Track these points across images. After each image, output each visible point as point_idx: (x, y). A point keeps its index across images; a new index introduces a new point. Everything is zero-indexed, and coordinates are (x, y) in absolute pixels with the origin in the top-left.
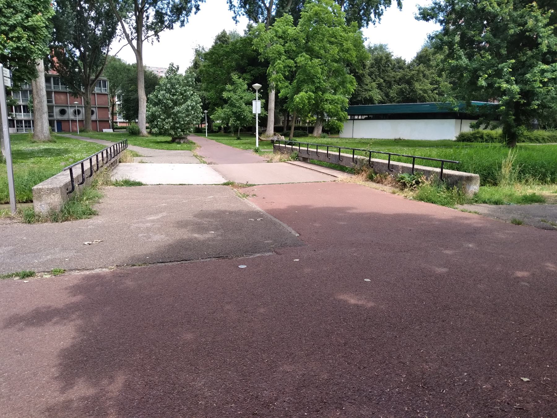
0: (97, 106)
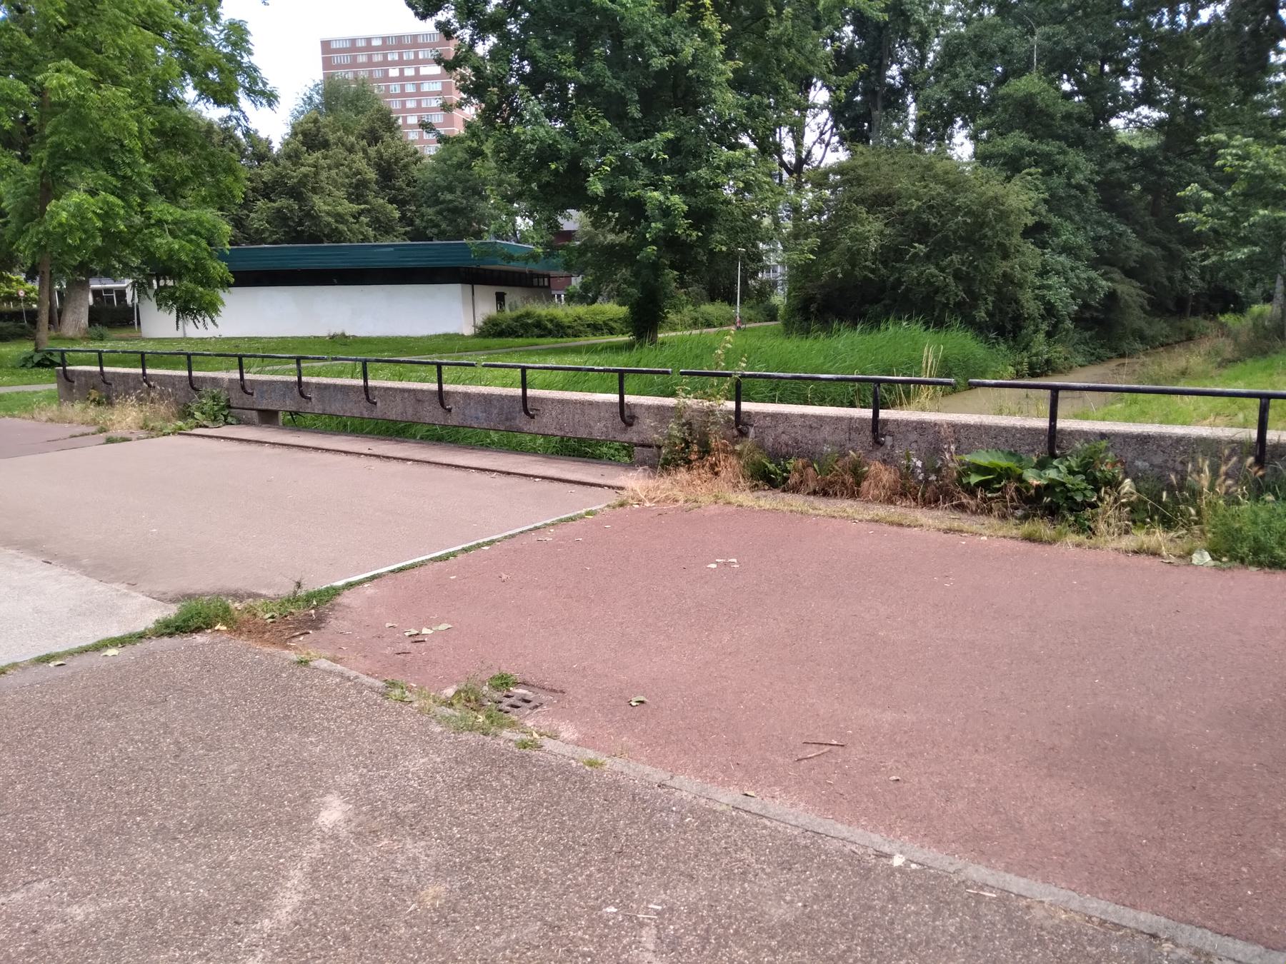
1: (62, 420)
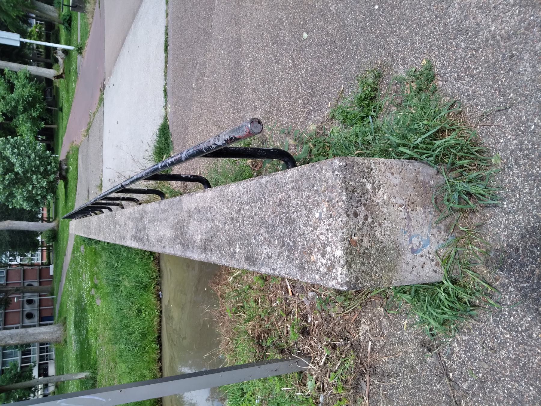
0: (22, 281)
1: (93, 12)
